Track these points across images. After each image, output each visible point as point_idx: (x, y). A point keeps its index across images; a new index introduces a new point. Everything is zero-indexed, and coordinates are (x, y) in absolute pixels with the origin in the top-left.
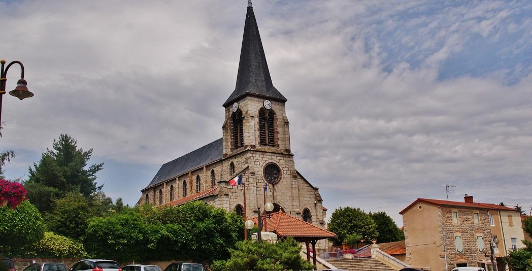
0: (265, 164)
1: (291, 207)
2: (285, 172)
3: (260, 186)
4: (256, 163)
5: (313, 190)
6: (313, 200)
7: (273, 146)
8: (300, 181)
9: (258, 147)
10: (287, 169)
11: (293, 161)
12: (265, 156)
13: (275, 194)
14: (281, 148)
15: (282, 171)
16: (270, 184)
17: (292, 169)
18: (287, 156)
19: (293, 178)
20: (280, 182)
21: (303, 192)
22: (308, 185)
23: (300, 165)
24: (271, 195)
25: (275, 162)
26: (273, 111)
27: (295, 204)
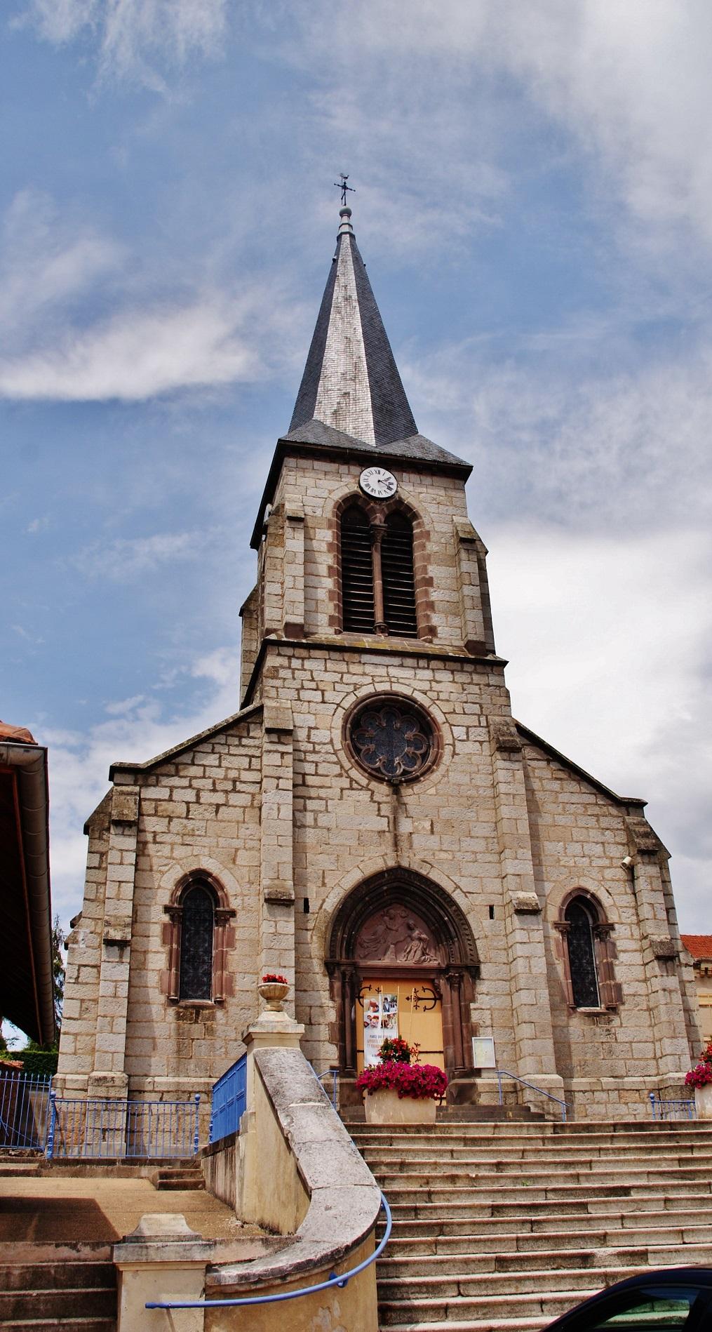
0: (351, 699)
1: (495, 885)
2: (459, 732)
3: (322, 793)
4: (305, 695)
5: (613, 811)
6: (616, 851)
7: (414, 636)
8: (541, 769)
9: (325, 632)
10: (473, 721)
11: (501, 687)
12: (355, 668)
13: (405, 826)
14: (448, 634)
15: (445, 729)
16: (381, 780)
17: (497, 719)
18: (469, 667)
19: (498, 755)
20: (435, 777)
21: (561, 820)
22: (585, 788)
23: (534, 702)
24: (381, 833)
25: (407, 691)
26: (409, 508)
27: (510, 867)
